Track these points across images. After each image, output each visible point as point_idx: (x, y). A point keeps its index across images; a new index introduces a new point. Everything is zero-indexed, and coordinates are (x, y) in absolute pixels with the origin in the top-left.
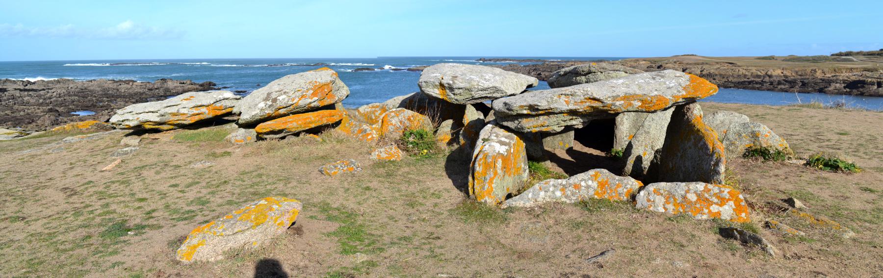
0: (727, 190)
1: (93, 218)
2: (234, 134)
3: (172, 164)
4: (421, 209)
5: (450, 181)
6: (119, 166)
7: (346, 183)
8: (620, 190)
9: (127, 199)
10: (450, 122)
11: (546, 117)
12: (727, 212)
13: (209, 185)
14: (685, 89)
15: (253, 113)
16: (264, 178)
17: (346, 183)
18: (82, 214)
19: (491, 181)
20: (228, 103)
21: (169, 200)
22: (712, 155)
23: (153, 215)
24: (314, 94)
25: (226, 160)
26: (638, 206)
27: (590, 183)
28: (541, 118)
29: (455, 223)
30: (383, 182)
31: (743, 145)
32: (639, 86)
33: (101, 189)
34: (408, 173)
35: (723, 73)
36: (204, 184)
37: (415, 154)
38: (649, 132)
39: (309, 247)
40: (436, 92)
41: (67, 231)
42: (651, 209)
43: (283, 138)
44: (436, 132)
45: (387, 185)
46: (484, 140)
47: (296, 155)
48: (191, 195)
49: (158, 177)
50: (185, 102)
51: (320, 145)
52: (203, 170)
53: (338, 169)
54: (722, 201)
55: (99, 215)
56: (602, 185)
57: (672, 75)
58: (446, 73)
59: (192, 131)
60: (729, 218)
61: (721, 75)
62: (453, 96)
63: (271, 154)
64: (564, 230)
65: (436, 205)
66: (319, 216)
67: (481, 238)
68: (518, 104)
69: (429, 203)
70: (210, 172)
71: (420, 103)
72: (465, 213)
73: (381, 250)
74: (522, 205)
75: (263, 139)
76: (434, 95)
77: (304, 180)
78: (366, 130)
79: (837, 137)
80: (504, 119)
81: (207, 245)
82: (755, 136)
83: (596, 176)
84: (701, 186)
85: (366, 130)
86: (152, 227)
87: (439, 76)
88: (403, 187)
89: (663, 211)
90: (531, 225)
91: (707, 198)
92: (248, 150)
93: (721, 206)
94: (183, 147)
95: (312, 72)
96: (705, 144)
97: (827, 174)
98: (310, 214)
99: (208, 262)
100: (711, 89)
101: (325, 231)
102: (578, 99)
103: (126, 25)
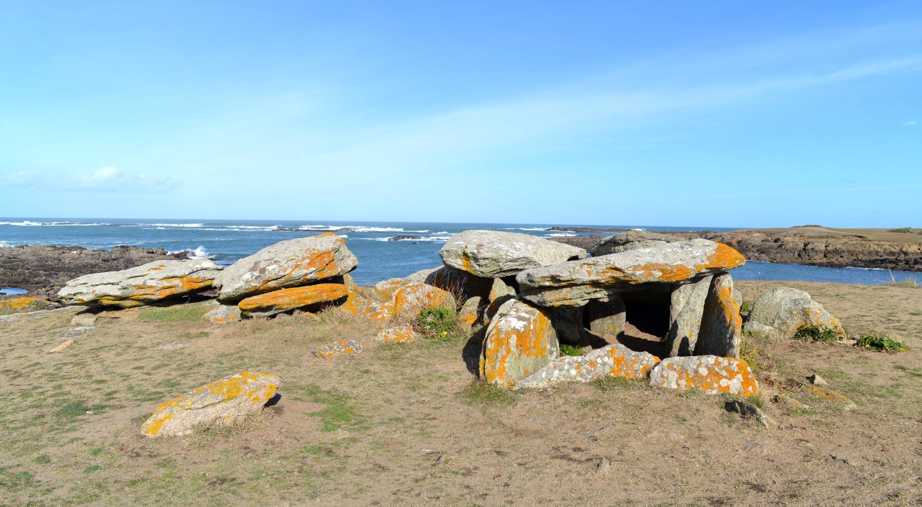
0: (736, 363)
1: (45, 399)
2: (213, 312)
3: (136, 345)
4: (423, 393)
5: (464, 364)
6: (70, 347)
7: (342, 366)
8: (636, 366)
9: (83, 381)
10: (476, 300)
11: (568, 289)
12: (734, 386)
13: (179, 368)
14: (709, 258)
15: (237, 286)
16: (246, 360)
17: (342, 366)
18: (31, 396)
19: (504, 358)
20: (207, 275)
21: (133, 382)
22: (728, 328)
23: (114, 396)
24: (311, 264)
25: (202, 342)
26: (652, 383)
27: (606, 359)
28: (564, 290)
29: (458, 405)
30: (385, 365)
31: (795, 324)
32: (665, 256)
33: (50, 371)
34: (418, 356)
35: (851, 249)
36: (174, 366)
37: (433, 337)
38: (694, 310)
39: (287, 426)
40: (458, 263)
41: (15, 411)
42: (665, 385)
43: (273, 316)
44: (459, 310)
45: (390, 368)
46: (502, 315)
47: (288, 336)
48: (159, 376)
49: (120, 359)
50: (153, 272)
51: (318, 324)
52: (175, 352)
53: (335, 350)
54: (731, 375)
55: (51, 396)
56: (618, 361)
57: (700, 244)
58: (470, 241)
59: (161, 309)
60: (736, 393)
61: (849, 251)
62: (477, 268)
63: (257, 335)
64: (571, 409)
65: (441, 388)
66: (305, 398)
67: (482, 419)
68: (540, 275)
69: (433, 387)
70: (182, 353)
71: (447, 278)
72: (472, 396)
73: (366, 428)
74: (534, 386)
75: (248, 318)
76: (457, 266)
77: (293, 362)
78: (375, 309)
79: (908, 317)
80: (524, 291)
81: (174, 420)
82: (805, 313)
83: (612, 351)
84: (711, 359)
85: (375, 309)
86: (113, 407)
87: (463, 244)
88: (408, 371)
89: (676, 387)
90: (538, 406)
91: (717, 372)
92: (229, 331)
93: (730, 379)
94: (150, 327)
95: (312, 238)
96: (724, 317)
97: (873, 354)
98: (295, 396)
99: (175, 436)
100: (736, 258)
101: (309, 412)
102: (600, 269)
103: (106, 172)
